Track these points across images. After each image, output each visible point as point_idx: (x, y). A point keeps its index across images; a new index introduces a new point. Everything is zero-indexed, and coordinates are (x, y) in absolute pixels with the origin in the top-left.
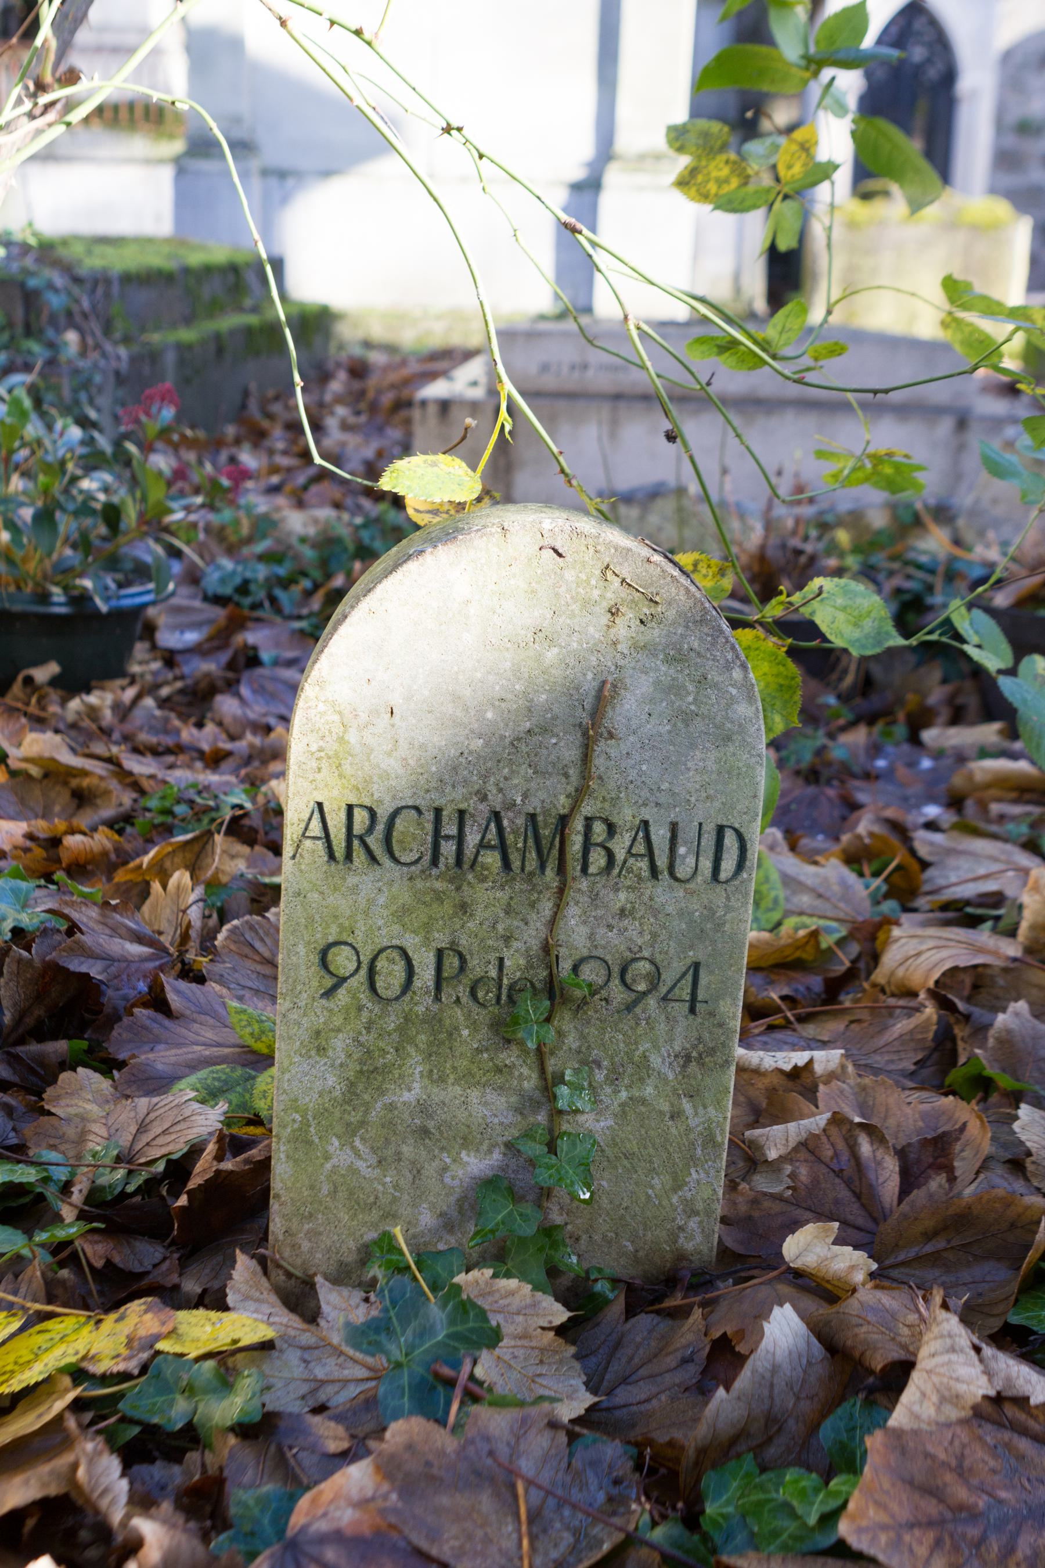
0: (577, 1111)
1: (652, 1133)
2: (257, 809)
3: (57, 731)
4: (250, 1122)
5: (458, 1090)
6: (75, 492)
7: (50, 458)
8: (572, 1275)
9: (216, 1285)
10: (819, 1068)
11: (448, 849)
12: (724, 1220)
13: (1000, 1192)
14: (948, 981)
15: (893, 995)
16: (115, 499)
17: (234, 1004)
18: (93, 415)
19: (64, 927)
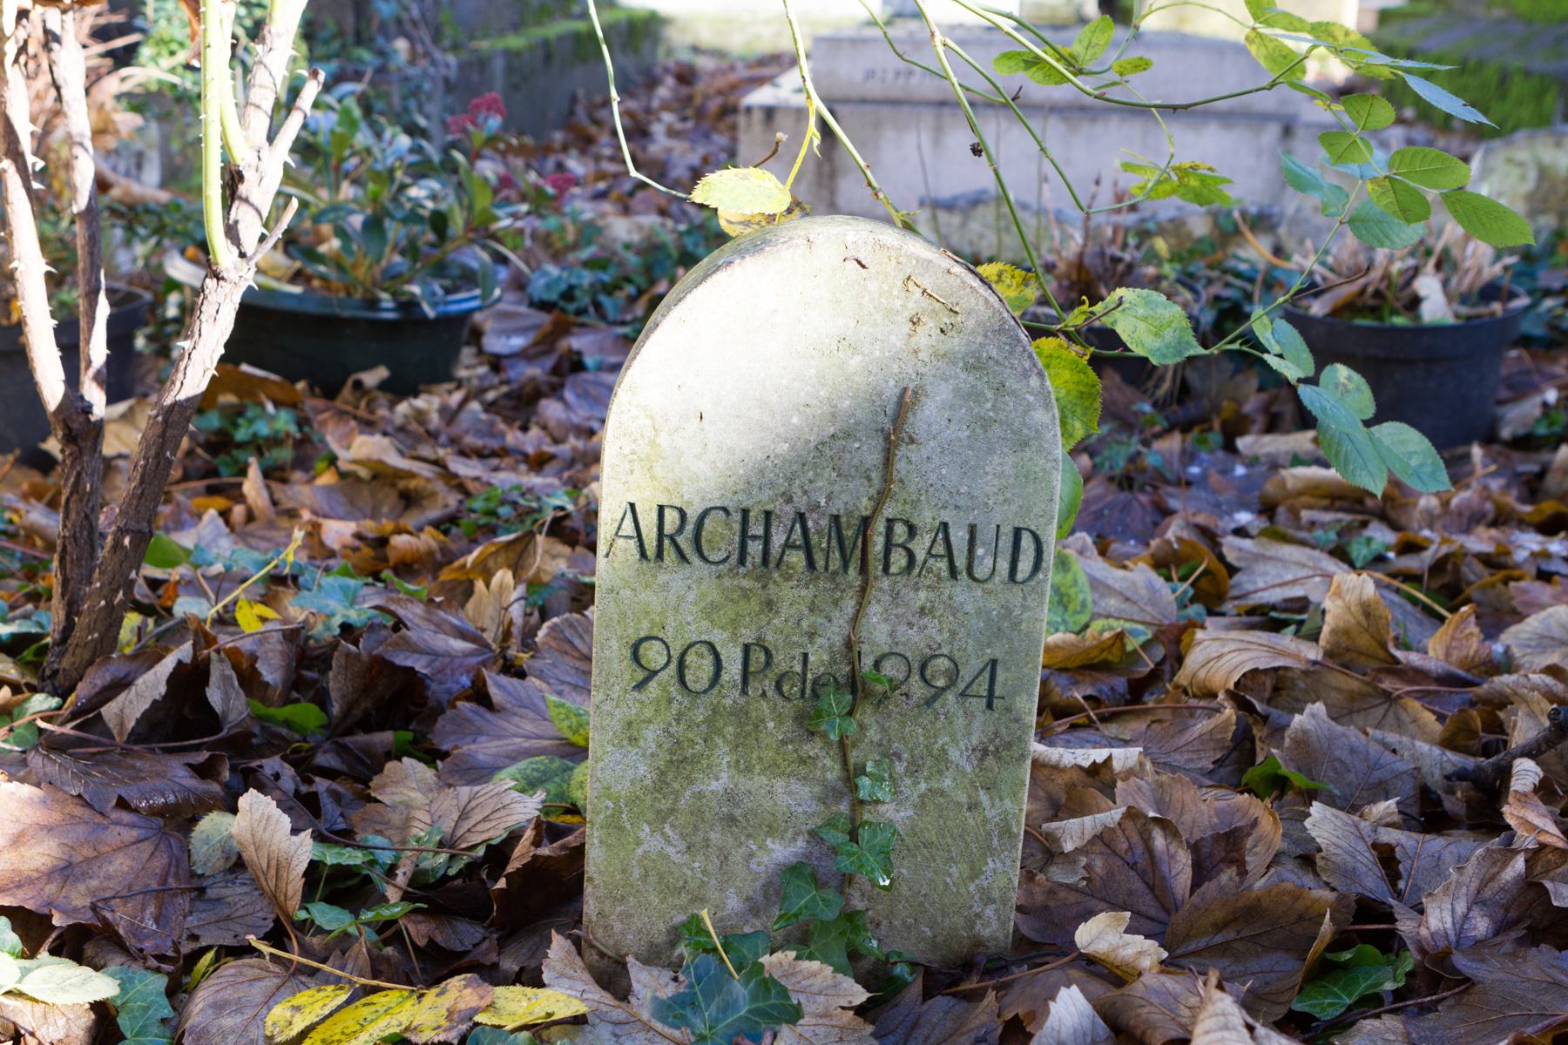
0: (877, 802)
1: (950, 823)
2: (579, 511)
3: (385, 434)
4: (568, 811)
5: (764, 780)
6: (403, 199)
7: (379, 167)
8: (873, 959)
9: (533, 964)
10: (1117, 765)
11: (755, 548)
12: (1019, 909)
13: (1289, 886)
14: (1249, 683)
15: (1195, 696)
16: (443, 207)
17: (553, 698)
18: (422, 122)
19: (390, 623)
